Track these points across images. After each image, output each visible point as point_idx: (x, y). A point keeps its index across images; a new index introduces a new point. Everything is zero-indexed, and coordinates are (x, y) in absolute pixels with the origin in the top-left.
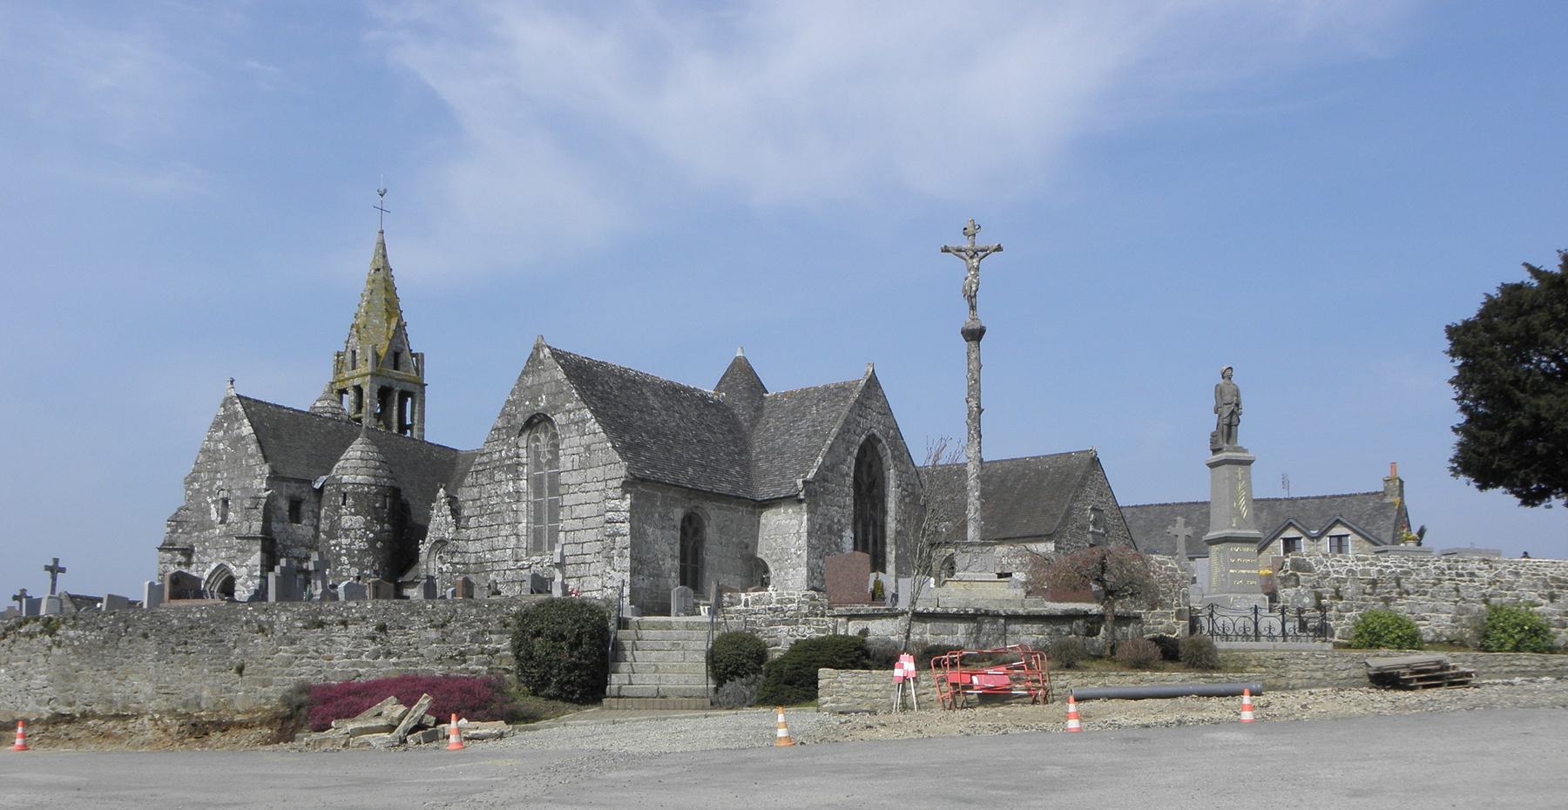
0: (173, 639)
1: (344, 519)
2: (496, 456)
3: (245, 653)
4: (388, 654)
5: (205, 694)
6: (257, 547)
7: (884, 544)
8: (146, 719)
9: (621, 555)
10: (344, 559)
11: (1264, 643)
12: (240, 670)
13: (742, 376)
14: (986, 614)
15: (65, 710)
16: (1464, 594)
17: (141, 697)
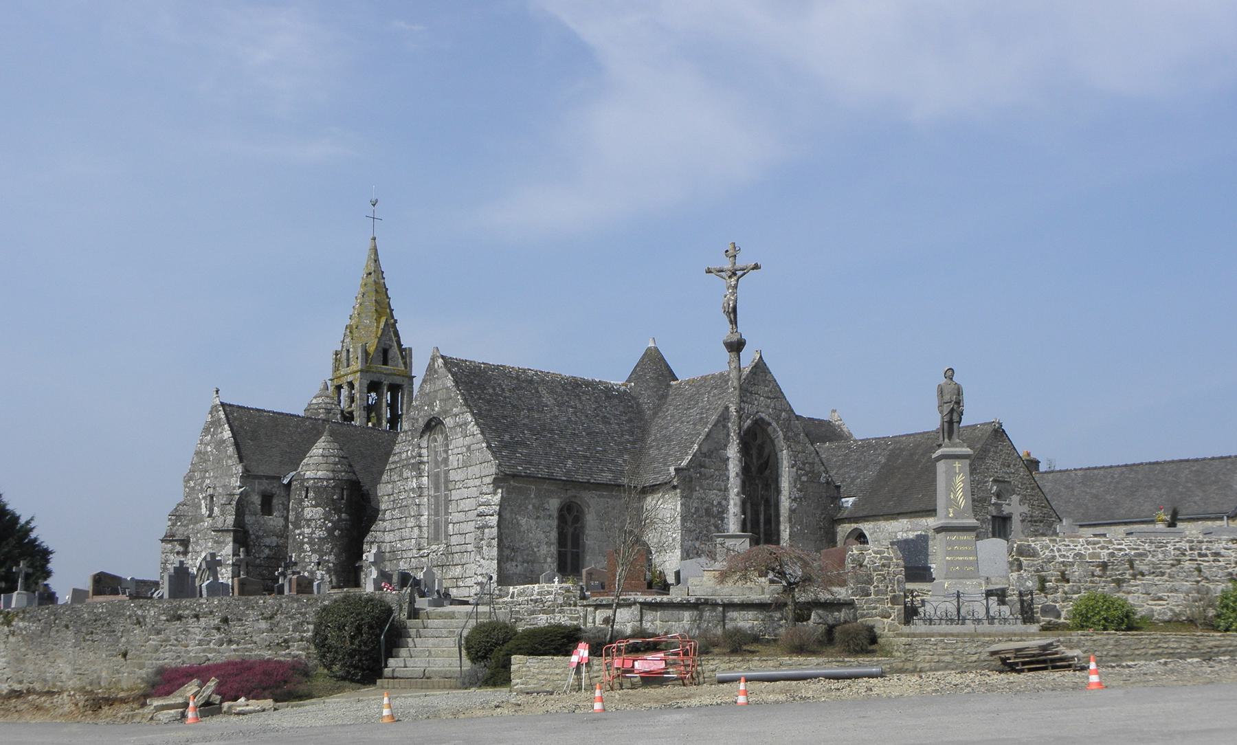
0: (84, 629)
1: (307, 510)
2: (404, 456)
3: (128, 642)
4: (230, 642)
5: (104, 674)
6: (229, 539)
7: (778, 523)
8: (65, 695)
9: (489, 545)
10: (306, 546)
11: (969, 627)
12: (125, 655)
13: (655, 368)
14: (706, 603)
15: (17, 687)
16: (1207, 573)
17: (64, 677)
